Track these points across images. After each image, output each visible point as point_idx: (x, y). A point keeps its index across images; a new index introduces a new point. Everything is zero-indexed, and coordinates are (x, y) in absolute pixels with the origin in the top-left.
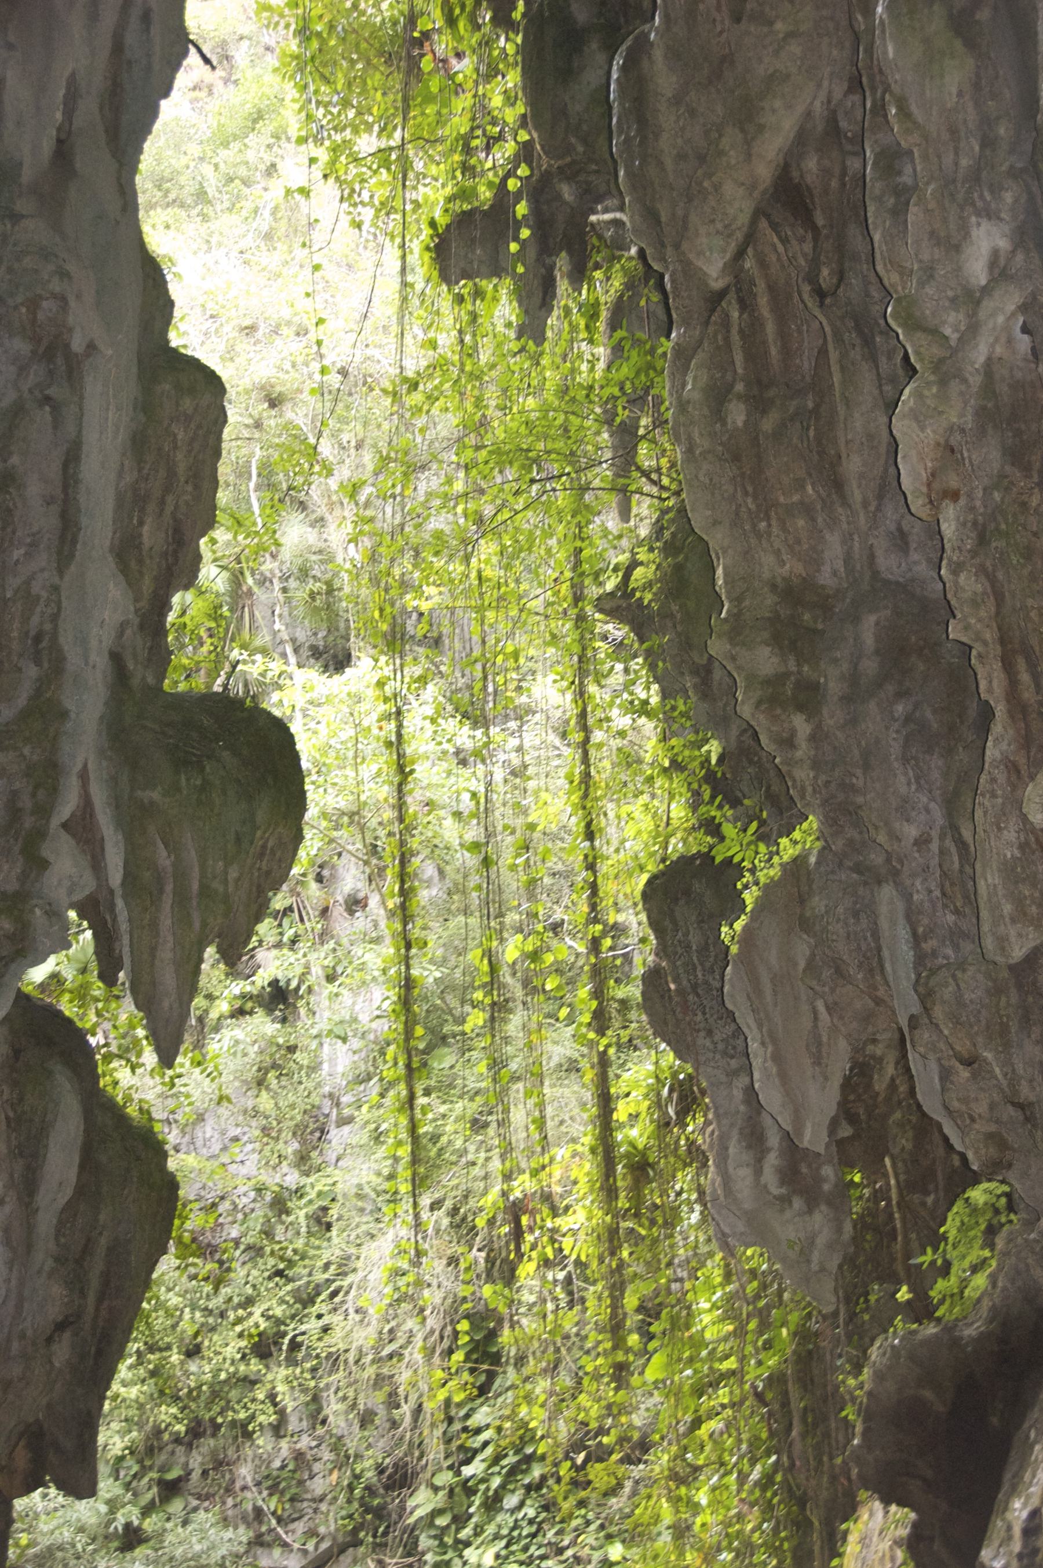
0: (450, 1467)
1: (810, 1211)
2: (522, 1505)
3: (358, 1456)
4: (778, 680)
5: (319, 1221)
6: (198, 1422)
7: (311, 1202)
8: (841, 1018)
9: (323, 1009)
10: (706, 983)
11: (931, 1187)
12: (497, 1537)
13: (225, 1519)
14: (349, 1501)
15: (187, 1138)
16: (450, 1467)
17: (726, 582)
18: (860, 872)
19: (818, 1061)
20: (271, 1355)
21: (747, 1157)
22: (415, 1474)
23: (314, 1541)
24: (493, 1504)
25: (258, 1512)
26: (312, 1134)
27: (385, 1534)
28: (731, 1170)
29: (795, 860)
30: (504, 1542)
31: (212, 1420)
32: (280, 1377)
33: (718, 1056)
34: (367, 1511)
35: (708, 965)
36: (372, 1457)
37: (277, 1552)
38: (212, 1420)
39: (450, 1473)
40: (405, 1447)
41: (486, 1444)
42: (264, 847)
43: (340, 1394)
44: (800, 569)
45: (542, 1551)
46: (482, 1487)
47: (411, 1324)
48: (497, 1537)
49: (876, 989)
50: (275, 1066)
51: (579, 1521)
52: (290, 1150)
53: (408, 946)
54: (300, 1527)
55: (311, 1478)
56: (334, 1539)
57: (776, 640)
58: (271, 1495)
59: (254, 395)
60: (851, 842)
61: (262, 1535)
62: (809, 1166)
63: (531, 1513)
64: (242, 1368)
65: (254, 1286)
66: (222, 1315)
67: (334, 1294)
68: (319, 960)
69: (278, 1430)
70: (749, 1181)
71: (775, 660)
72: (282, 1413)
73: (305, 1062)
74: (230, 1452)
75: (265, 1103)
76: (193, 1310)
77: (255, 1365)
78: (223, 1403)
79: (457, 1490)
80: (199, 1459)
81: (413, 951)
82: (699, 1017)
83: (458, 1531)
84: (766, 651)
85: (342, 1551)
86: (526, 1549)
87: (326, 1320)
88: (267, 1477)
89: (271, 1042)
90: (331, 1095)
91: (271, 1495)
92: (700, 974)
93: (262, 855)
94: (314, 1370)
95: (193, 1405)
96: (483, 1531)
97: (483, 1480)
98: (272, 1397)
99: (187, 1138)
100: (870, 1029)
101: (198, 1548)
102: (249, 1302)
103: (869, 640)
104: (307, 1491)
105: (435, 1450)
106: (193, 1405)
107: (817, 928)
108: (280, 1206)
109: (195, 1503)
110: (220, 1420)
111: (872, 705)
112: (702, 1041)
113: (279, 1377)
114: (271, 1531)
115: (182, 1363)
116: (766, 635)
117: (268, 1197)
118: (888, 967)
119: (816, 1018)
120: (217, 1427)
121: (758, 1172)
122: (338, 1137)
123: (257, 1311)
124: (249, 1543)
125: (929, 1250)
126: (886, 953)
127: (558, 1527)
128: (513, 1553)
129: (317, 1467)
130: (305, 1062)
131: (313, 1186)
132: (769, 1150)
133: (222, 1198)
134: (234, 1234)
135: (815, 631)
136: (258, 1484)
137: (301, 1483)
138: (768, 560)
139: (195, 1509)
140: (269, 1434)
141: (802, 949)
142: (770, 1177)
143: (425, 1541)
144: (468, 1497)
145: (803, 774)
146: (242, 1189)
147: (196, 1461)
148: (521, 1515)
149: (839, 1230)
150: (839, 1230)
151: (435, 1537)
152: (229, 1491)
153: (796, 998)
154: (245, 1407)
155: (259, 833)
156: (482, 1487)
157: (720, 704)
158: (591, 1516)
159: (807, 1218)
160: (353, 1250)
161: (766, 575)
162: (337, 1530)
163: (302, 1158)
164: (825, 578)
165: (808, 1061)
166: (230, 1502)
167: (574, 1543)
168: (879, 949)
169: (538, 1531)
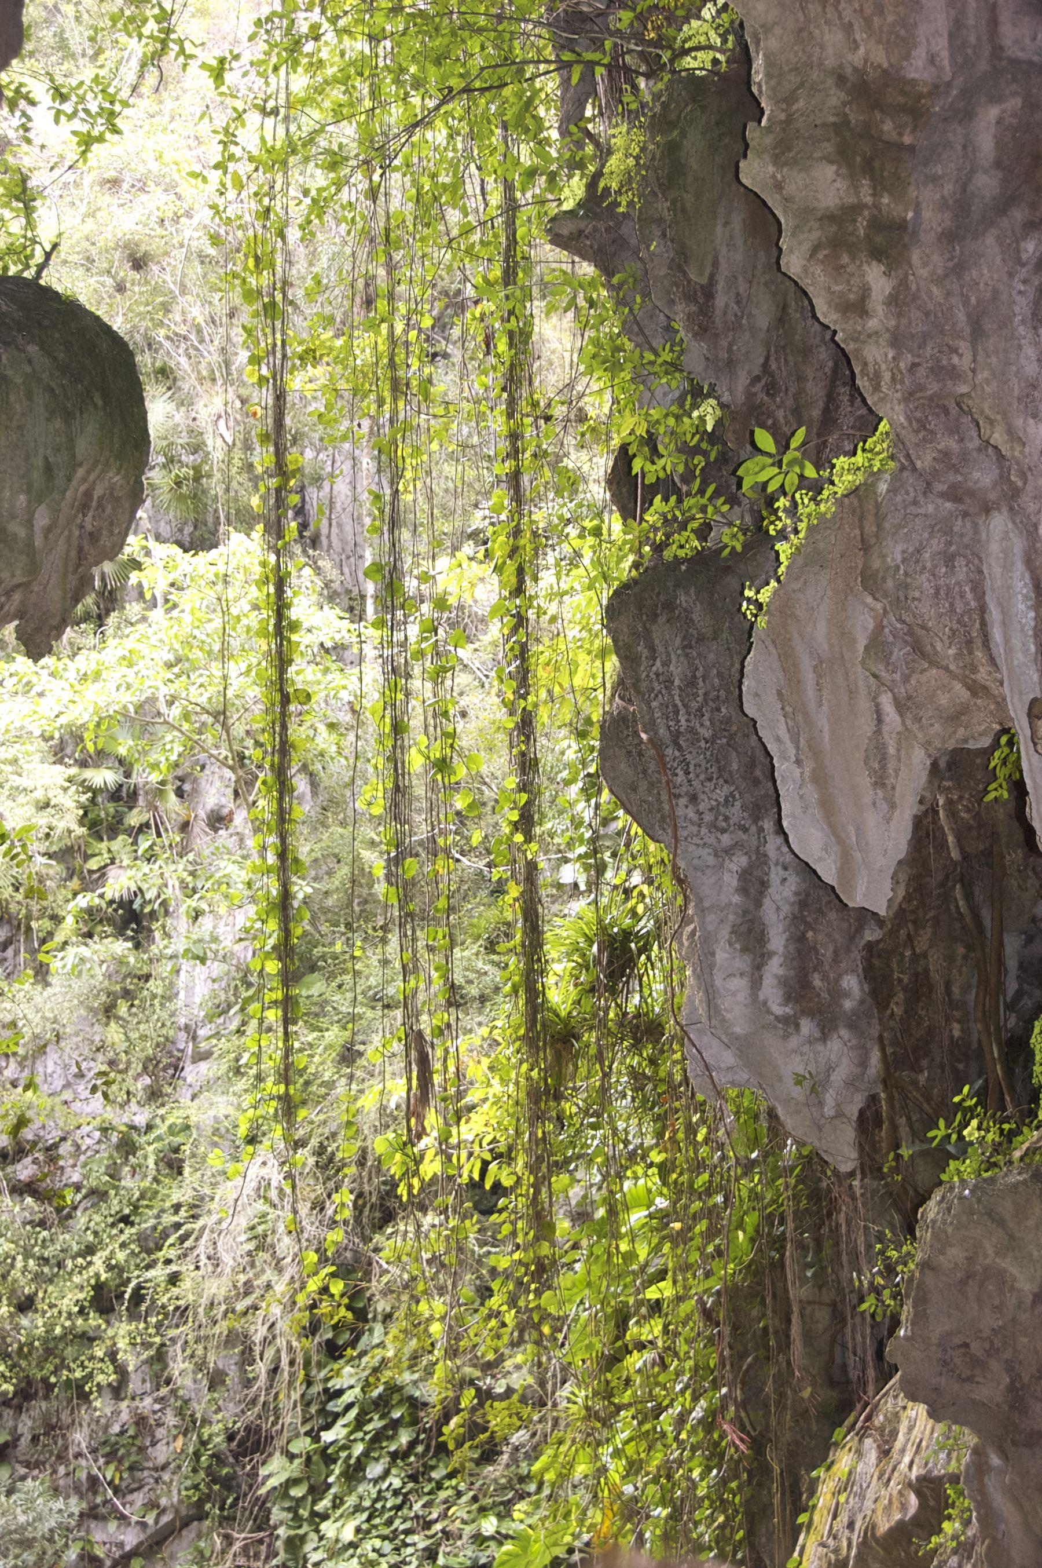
0: (307, 1434)
1: (824, 1038)
2: (387, 1473)
3: (206, 1421)
4: (840, 218)
5: (170, 1165)
6: (29, 1381)
7: (159, 1138)
8: (918, 719)
9: (175, 936)
10: (691, 730)
11: (924, 1063)
12: (358, 1509)
13: (56, 1490)
14: (195, 1471)
15: (26, 1073)
16: (307, 1434)
17: (768, 75)
18: (957, 499)
19: (880, 782)
20: (113, 1310)
21: (742, 963)
22: (270, 1439)
23: (155, 1512)
24: (354, 1473)
25: (93, 1481)
26: (164, 1070)
27: (234, 1505)
28: (718, 982)
29: (854, 492)
30: (365, 1515)
31: (45, 1380)
32: (121, 1332)
33: (704, 830)
34: (214, 1481)
35: (694, 705)
36: (222, 1419)
37: (112, 1526)
38: (45, 1380)
39: (308, 1440)
40: (259, 1407)
41: (349, 1407)
42: (88, 494)
43: (188, 1352)
44: (880, 57)
45: (408, 1525)
46: (343, 1454)
47: (269, 1275)
48: (358, 1509)
49: (974, 670)
50: (123, 995)
51: (450, 1492)
52: (139, 1085)
53: (286, 700)
54: (139, 1498)
55: (154, 1444)
56: (177, 1511)
57: (843, 156)
58: (107, 1463)
59: (117, 255)
60: (946, 454)
61: (97, 1506)
62: (825, 978)
63: (397, 1483)
64: (80, 1322)
65: (96, 1233)
66: (60, 1265)
67: (182, 1239)
68: (175, 872)
69: (117, 1391)
70: (743, 996)
71: (841, 184)
72: (121, 1371)
73: (159, 991)
74: (63, 1417)
75: (114, 1033)
76: (25, 1259)
77: (95, 1320)
78: (57, 1361)
79: (315, 1458)
80: (30, 1423)
81: (292, 707)
82: (681, 778)
83: (314, 1502)
84: (830, 170)
85: (186, 1524)
86: (389, 1522)
87: (174, 1268)
88: (105, 1443)
89: (121, 962)
90: (187, 1027)
91: (107, 1463)
92: (683, 719)
93: (85, 507)
94: (159, 1326)
95: (23, 1363)
96: (342, 1503)
97: (344, 1448)
98: (112, 1355)
99: (26, 1073)
100: (961, 732)
101: (22, 1519)
102: (90, 1250)
103: (986, 143)
104: (148, 1459)
105: (291, 1418)
106: (23, 1363)
107: (890, 584)
108: (127, 1147)
109: (23, 1471)
110: (53, 1380)
111: (990, 240)
112: (684, 810)
113: (121, 1332)
114: (106, 1502)
115: (11, 1315)
116: (828, 148)
117: (115, 1138)
118: (997, 634)
119: (880, 721)
120: (50, 1387)
121: (756, 984)
122: (194, 1073)
123: (98, 1261)
124: (81, 1515)
125: (942, 1123)
126: (994, 614)
127: (426, 1498)
128: (375, 1527)
129: (160, 1433)
130: (159, 991)
131: (163, 1119)
132: (771, 954)
133: (63, 1139)
134: (76, 1178)
135: (901, 147)
136: (94, 1451)
137: (142, 1450)
138: (833, 39)
139: (23, 1478)
140: (108, 1395)
141: (863, 622)
142: (771, 992)
143: (277, 1514)
144: (327, 1466)
145: (876, 354)
146: (85, 1129)
147: (26, 1426)
148: (385, 1486)
149: (864, 1064)
150: (864, 1064)
151: (289, 1509)
152: (61, 1458)
153: (852, 693)
154: (83, 1366)
155: (81, 472)
156: (343, 1454)
157: (724, 343)
158: (462, 1486)
159: (820, 1047)
160: (207, 1191)
161: (830, 63)
162: (180, 1501)
163: (153, 1093)
164: (917, 69)
165: (865, 781)
166: (62, 1470)
167: (444, 1516)
168: (983, 609)
169: (404, 1502)
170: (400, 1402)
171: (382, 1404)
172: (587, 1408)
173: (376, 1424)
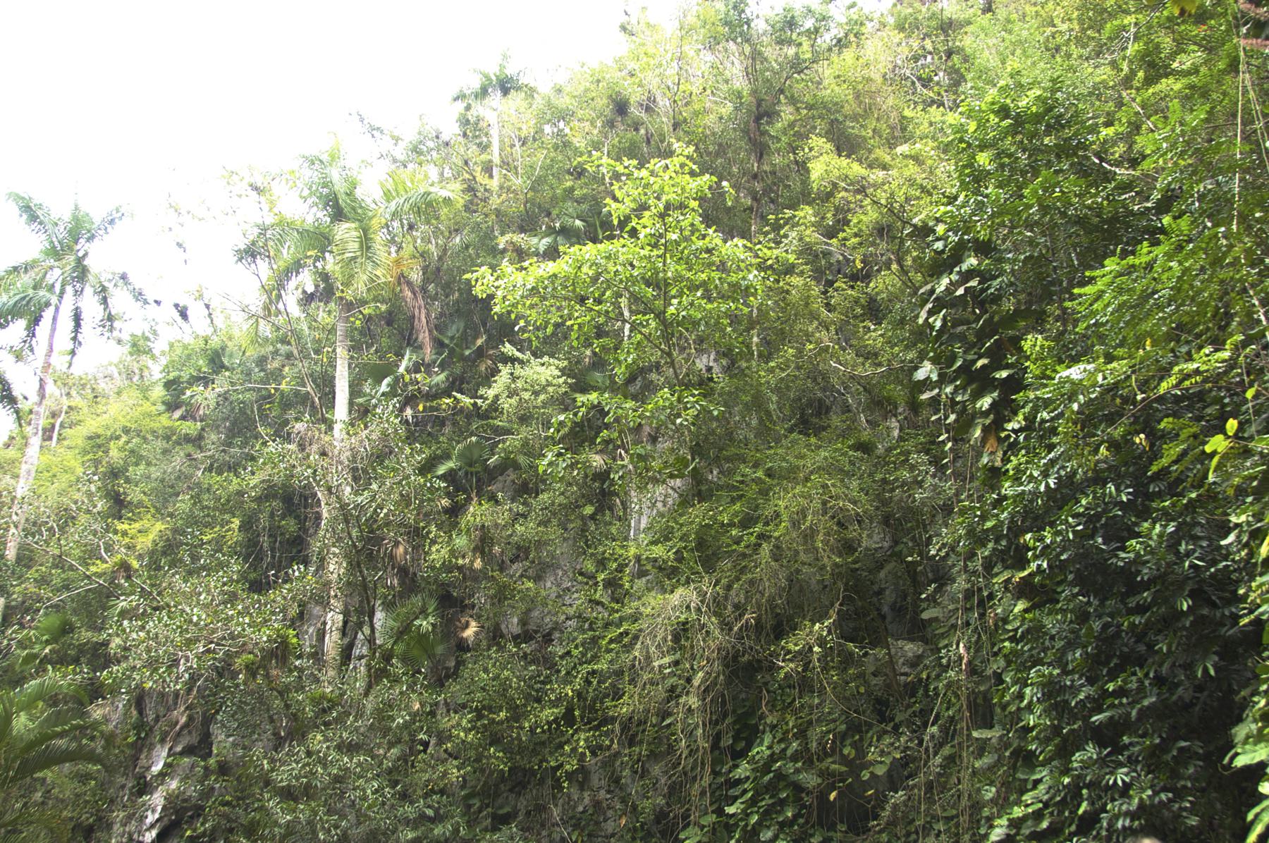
55: (605, 820)
88: (571, 818)
104: (602, 830)
129: (610, 813)
137: (597, 823)
166: (544, 833)
170: (786, 787)
171: (771, 788)
172: (919, 630)
173: (766, 801)
